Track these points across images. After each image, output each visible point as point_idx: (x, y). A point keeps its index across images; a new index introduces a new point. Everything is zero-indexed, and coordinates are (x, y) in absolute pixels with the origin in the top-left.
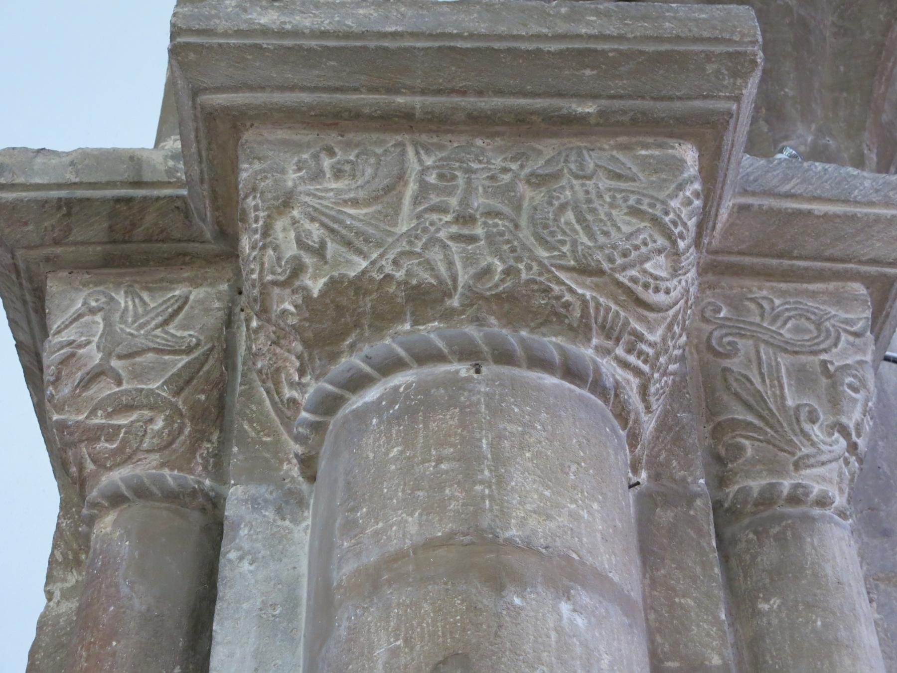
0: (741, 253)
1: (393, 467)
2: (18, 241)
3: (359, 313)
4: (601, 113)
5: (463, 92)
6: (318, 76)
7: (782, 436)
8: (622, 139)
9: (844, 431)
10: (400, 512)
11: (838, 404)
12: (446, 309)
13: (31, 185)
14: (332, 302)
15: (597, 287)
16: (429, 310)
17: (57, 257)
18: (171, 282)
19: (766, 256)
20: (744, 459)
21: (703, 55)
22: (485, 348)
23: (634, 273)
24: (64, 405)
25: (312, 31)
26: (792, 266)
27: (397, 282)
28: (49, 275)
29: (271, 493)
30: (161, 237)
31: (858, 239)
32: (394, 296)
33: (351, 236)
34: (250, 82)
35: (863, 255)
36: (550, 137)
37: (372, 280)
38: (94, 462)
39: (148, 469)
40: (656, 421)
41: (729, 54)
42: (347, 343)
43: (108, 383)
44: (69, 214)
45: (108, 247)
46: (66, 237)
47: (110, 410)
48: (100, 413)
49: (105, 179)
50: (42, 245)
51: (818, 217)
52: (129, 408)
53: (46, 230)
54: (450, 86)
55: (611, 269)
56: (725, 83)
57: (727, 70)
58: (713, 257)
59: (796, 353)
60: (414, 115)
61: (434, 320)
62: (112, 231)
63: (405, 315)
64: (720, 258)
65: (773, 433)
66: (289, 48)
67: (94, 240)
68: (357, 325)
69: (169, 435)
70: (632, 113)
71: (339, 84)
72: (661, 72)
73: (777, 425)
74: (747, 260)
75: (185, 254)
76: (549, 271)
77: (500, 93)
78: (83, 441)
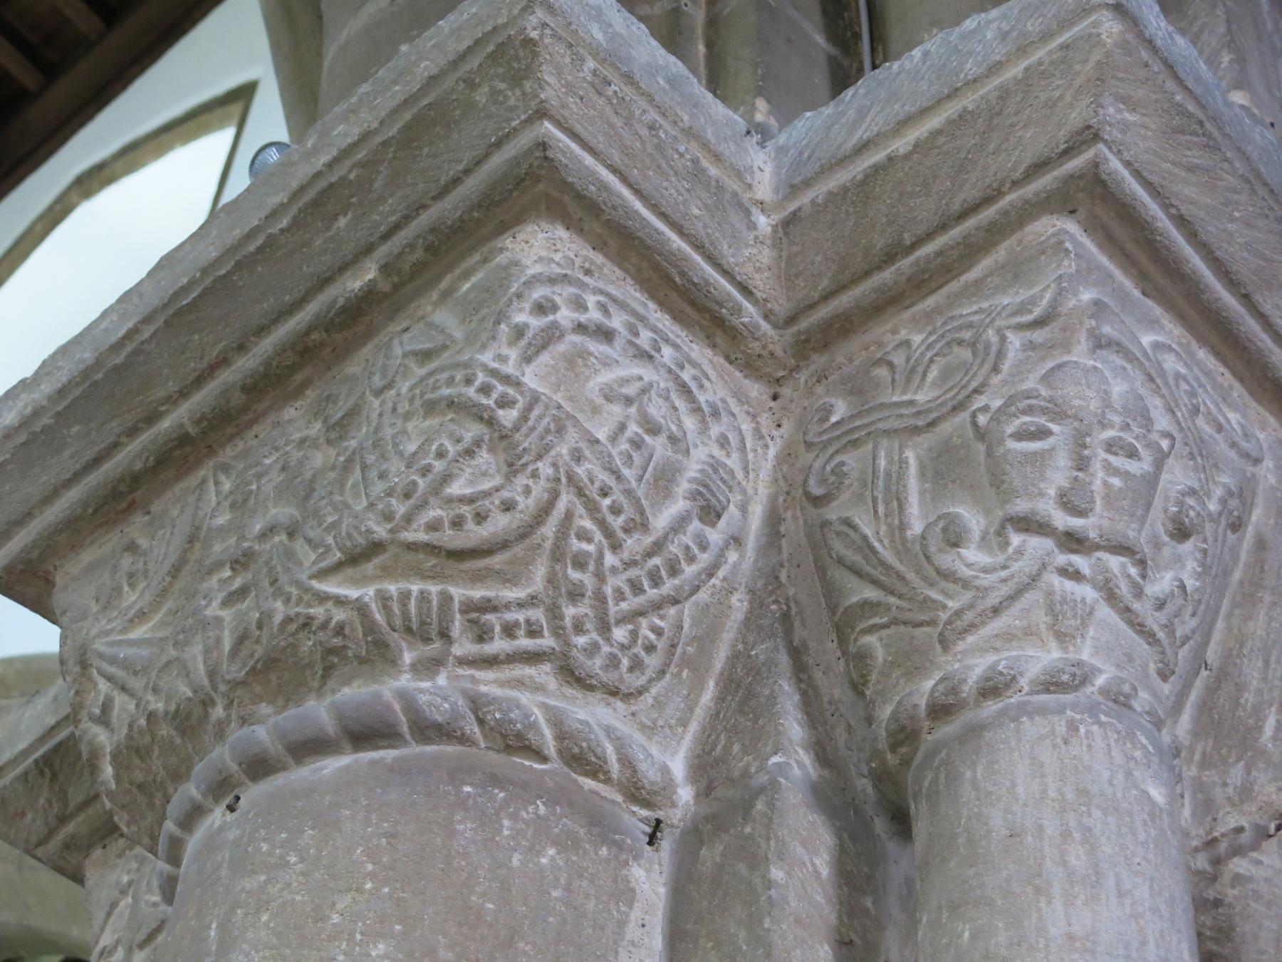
0: (828, 296)
4: (385, 269)
5: (223, 362)
6: (72, 457)
9: (1031, 525)
11: (1003, 482)
15: (386, 572)
17: (73, 837)
19: (867, 274)
20: (876, 671)
23: (433, 513)
26: (917, 261)
31: (991, 147)
35: (1014, 169)
40: (717, 684)
41: (492, 56)
44: (54, 776)
46: (66, 805)
51: (907, 157)
55: (391, 531)
56: (512, 102)
57: (503, 81)
58: (794, 329)
59: (932, 424)
60: (187, 434)
64: (804, 324)
65: (898, 602)
72: (426, 150)
73: (898, 585)
74: (845, 300)
77: (262, 330)
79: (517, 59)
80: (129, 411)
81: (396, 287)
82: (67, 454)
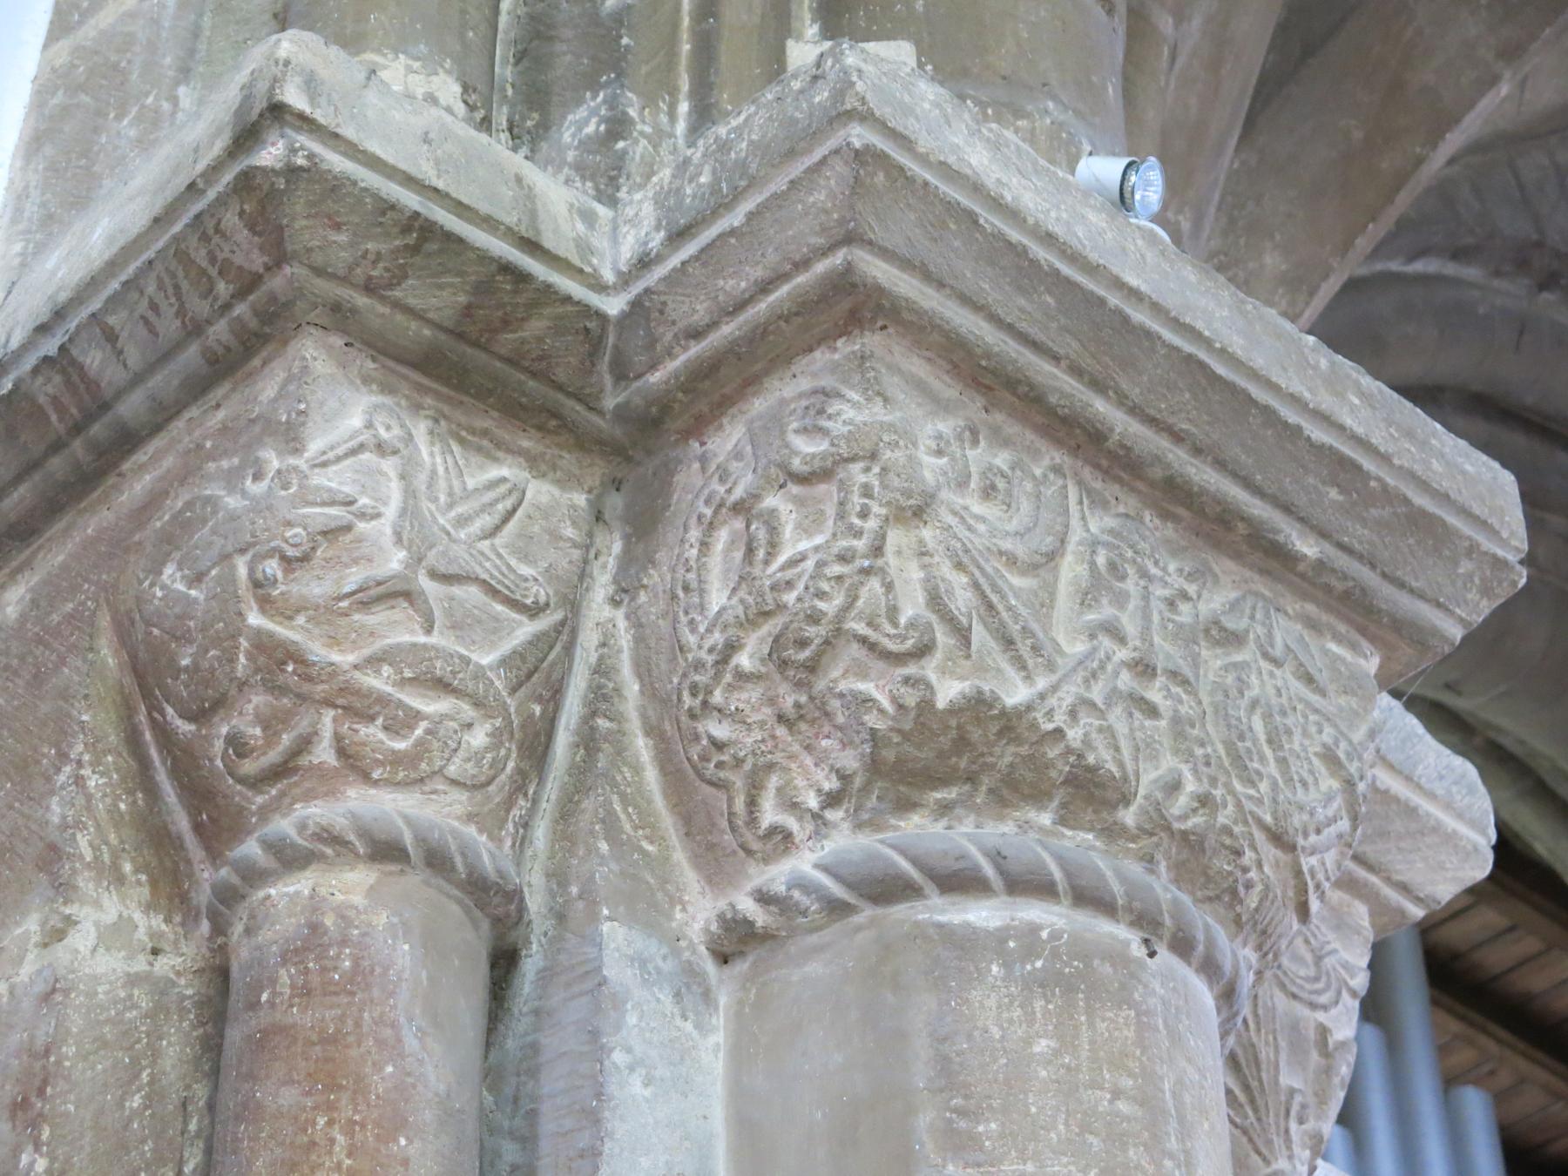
1: (1044, 1073)
2: (309, 250)
3: (985, 764)
4: (1320, 565)
5: (1178, 437)
6: (1022, 310)
7: (1264, 1130)
8: (1311, 608)
10: (1065, 1160)
12: (1115, 823)
13: (364, 152)
14: (959, 727)
16: (1090, 809)
17: (354, 311)
18: (499, 445)
21: (1467, 544)
22: (1168, 921)
24: (298, 611)
25: (1037, 224)
27: (1067, 746)
28: (313, 330)
29: (665, 958)
30: (536, 366)
32: (1049, 765)
33: (1014, 629)
34: (932, 268)
36: (1231, 557)
37: (1034, 726)
38: (342, 752)
39: (448, 816)
42: (938, 795)
43: (410, 619)
44: (415, 249)
45: (443, 337)
46: (390, 286)
47: (408, 674)
48: (386, 670)
49: (484, 207)
50: (344, 280)
52: (443, 686)
53: (364, 256)
54: (1171, 420)
56: (1469, 596)
59: (1294, 996)
60: (1106, 439)
61: (1091, 830)
62: (468, 316)
63: (1051, 799)
66: (1010, 243)
67: (431, 315)
68: (972, 779)
69: (491, 767)
70: (1351, 584)
71: (1040, 337)
72: (1411, 541)
73: (1263, 1110)
75: (555, 415)
76: (1246, 822)
77: (1221, 464)
78: (336, 707)
79: (1500, 583)
80: (1093, 356)
81: (1303, 576)
82: (1022, 302)
